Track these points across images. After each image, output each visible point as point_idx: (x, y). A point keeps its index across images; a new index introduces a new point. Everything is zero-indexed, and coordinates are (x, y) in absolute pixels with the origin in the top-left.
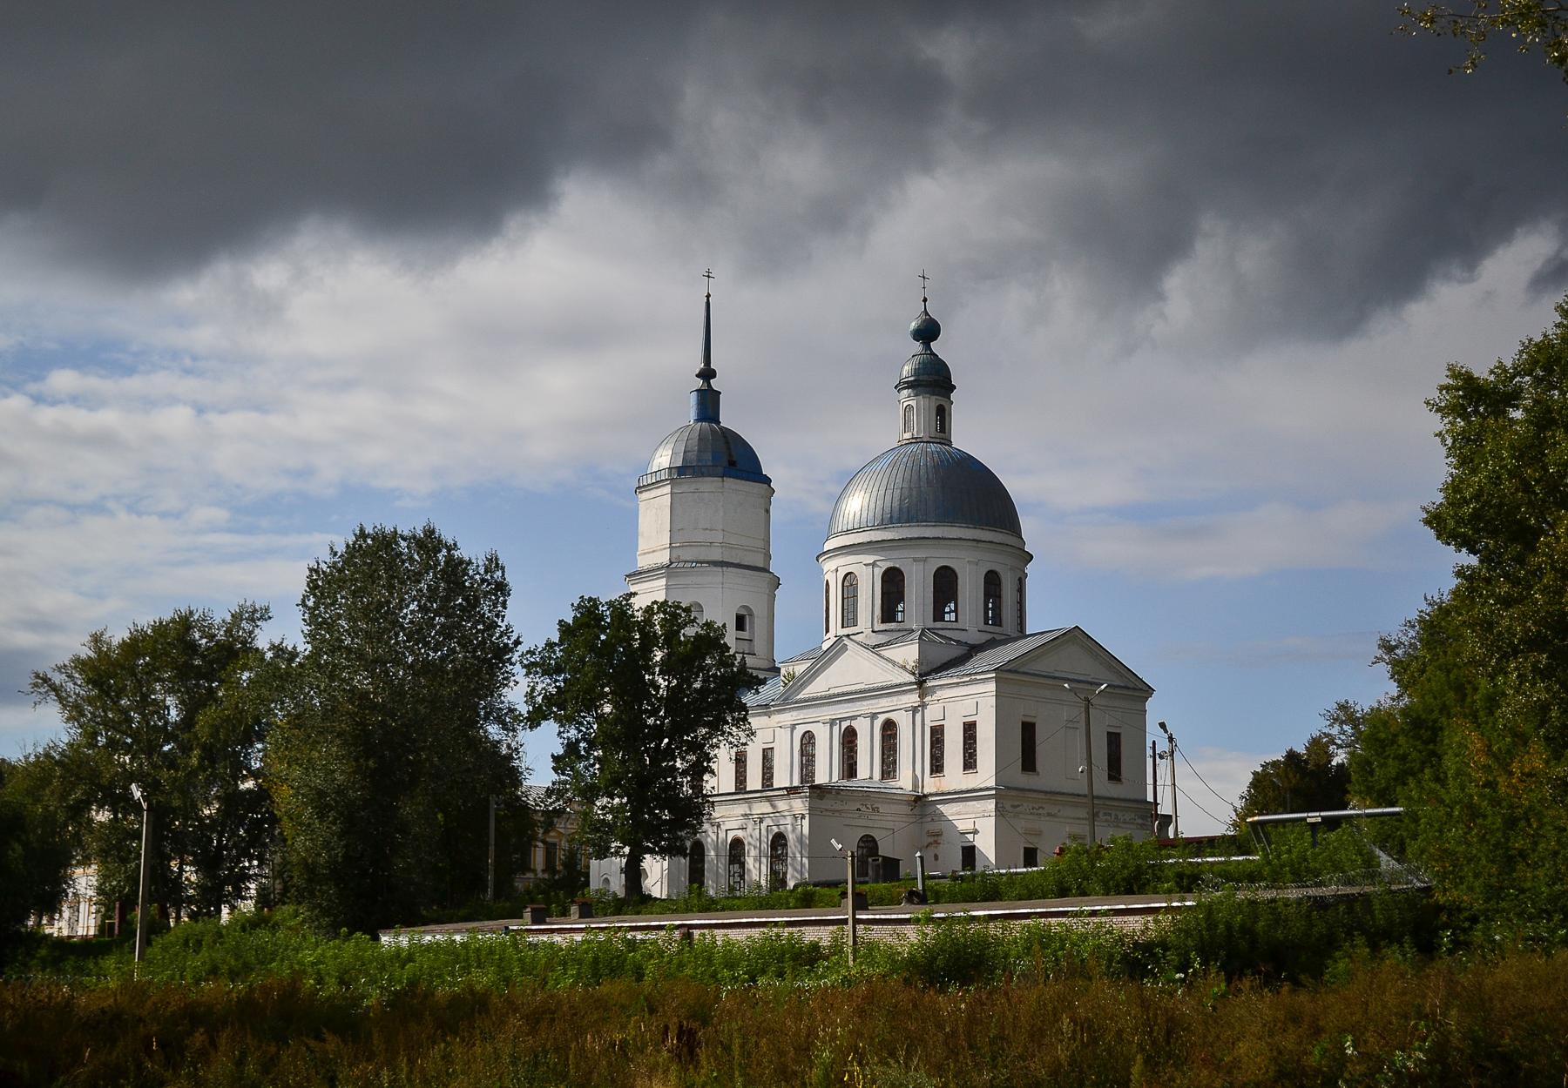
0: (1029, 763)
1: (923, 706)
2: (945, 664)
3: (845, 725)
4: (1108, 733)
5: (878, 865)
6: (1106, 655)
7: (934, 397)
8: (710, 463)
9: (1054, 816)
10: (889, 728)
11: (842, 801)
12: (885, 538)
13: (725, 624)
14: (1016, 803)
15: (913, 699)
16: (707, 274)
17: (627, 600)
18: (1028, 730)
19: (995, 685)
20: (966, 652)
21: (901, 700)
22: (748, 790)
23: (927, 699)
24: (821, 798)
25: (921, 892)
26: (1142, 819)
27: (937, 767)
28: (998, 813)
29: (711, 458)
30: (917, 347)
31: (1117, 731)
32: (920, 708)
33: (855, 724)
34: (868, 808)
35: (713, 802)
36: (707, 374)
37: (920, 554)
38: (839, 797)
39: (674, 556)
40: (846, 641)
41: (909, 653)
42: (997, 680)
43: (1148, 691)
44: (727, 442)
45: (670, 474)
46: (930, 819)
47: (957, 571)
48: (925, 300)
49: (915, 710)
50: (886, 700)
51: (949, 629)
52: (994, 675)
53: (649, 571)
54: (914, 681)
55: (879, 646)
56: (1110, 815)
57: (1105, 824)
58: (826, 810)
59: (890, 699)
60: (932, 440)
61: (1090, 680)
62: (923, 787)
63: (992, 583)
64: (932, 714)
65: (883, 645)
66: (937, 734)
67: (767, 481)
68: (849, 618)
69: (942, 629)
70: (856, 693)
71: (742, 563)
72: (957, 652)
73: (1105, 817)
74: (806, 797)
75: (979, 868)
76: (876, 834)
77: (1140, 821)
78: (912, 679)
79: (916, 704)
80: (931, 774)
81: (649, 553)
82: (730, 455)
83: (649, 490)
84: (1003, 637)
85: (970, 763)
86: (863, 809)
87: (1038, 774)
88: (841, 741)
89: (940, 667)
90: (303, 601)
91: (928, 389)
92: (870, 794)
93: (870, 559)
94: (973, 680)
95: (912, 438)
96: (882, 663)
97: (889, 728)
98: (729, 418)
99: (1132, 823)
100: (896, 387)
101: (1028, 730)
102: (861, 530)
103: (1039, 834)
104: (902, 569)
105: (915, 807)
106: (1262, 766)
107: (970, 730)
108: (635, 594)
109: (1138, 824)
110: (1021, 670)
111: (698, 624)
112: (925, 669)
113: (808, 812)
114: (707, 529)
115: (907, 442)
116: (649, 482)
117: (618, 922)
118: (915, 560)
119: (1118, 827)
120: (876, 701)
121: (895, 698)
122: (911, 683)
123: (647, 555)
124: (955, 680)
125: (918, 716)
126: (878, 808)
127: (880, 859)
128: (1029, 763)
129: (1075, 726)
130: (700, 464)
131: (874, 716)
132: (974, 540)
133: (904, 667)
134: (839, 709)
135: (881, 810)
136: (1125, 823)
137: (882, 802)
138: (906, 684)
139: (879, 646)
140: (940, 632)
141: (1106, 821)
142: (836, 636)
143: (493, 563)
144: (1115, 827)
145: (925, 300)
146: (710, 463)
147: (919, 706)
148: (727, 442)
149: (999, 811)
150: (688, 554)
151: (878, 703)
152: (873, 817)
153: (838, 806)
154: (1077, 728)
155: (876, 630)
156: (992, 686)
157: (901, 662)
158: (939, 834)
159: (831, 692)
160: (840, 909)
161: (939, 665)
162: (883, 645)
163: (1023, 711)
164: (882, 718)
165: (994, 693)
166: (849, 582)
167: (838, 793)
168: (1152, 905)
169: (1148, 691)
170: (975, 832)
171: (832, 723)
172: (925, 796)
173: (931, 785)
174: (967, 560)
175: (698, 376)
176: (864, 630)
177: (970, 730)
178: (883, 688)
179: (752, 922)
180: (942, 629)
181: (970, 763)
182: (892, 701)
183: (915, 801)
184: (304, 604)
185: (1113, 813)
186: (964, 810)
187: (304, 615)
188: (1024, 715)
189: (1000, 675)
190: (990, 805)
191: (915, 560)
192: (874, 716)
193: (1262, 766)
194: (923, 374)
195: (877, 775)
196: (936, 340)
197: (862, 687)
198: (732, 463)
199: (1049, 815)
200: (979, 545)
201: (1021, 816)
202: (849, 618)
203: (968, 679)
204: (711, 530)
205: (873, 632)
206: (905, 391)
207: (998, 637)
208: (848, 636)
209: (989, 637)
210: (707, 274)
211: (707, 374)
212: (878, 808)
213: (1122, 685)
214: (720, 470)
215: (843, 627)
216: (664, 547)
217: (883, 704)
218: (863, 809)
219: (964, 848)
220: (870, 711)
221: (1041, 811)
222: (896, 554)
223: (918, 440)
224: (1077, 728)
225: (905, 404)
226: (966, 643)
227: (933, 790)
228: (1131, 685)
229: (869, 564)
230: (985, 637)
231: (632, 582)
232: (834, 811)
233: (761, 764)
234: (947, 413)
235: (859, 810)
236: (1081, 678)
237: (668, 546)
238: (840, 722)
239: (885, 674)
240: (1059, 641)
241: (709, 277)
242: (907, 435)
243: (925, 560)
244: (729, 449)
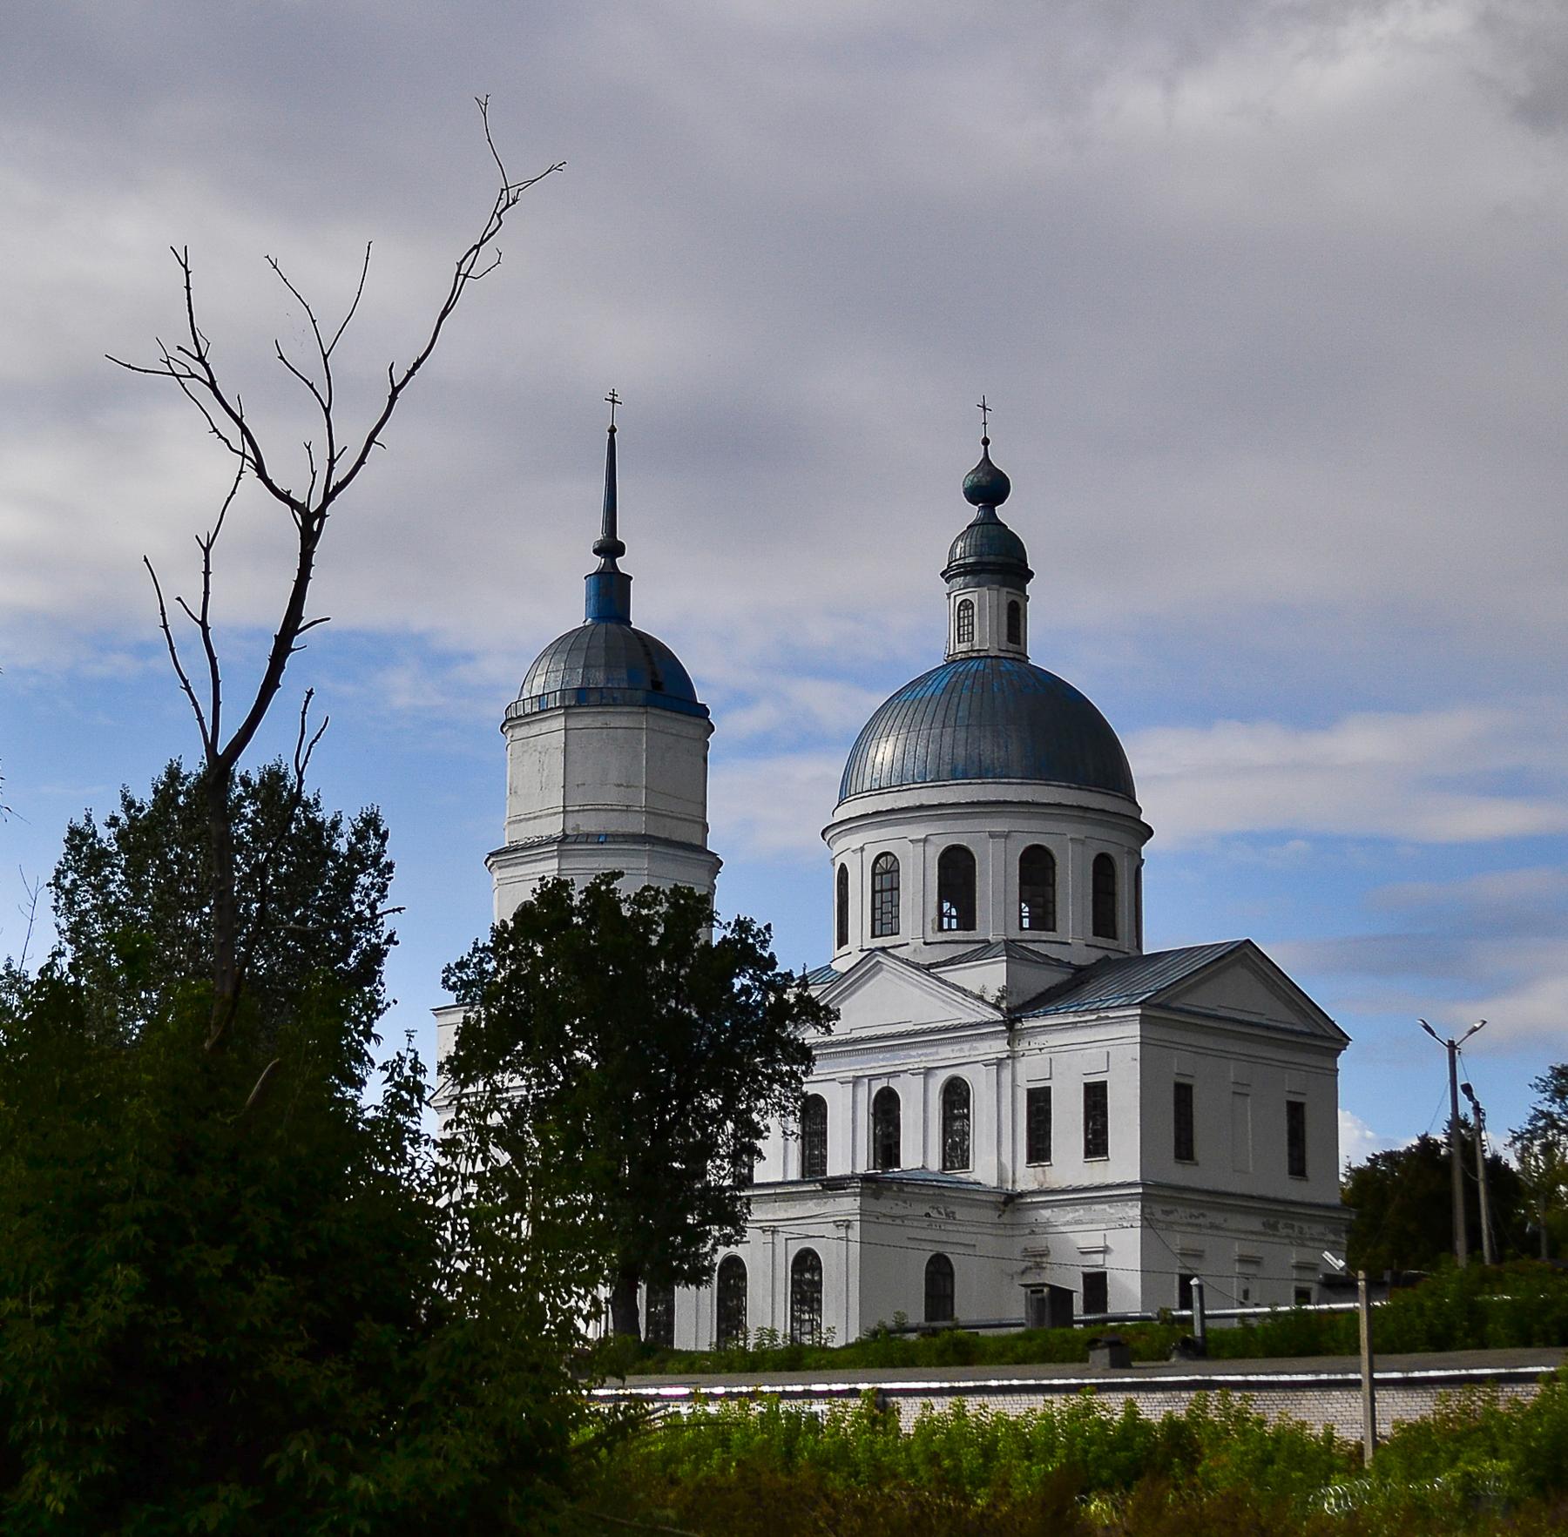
0: (1184, 1150)
1: (1014, 1058)
2: (1042, 994)
3: (877, 1086)
4: (1289, 1103)
5: (1043, 1300)
6: (1286, 985)
7: (1006, 589)
8: (624, 685)
9: (1218, 1228)
10: (956, 1095)
11: (905, 1202)
12: (943, 801)
13: (770, 924)
14: (1168, 1208)
15: (998, 1047)
16: (610, 397)
17: (608, 884)
18: (1183, 1095)
19: (1138, 1026)
20: (1070, 976)
21: (976, 1049)
22: (755, 1181)
23: (1022, 1046)
24: (877, 1195)
25: (1200, 1341)
26: (1335, 1235)
27: (1039, 1150)
28: (1145, 1223)
29: (625, 677)
30: (973, 512)
31: (1299, 1099)
32: (1010, 1061)
33: (894, 1084)
34: (940, 1213)
35: (749, 1198)
36: (610, 548)
37: (1000, 825)
38: (902, 1195)
39: (570, 825)
40: (881, 957)
41: (992, 976)
42: (1144, 1020)
43: (1341, 1040)
44: (648, 654)
45: (563, 698)
46: (1027, 1231)
47: (1054, 852)
48: (986, 442)
49: (999, 1063)
50: (950, 1048)
51: (1045, 942)
52: (1139, 1011)
53: (531, 847)
54: (1002, 1018)
55: (937, 965)
56: (1292, 1227)
57: (1286, 1241)
58: (884, 1215)
59: (957, 1047)
60: (1002, 655)
61: (1265, 1022)
62: (1014, 1182)
63: (1103, 869)
64: (1030, 1071)
65: (945, 964)
66: (1039, 1102)
67: (702, 712)
68: (884, 919)
69: (1034, 941)
70: (900, 1035)
71: (674, 839)
72: (1056, 977)
73: (1286, 1230)
74: (855, 1195)
75: (1114, 1308)
76: (946, 1250)
77: (1332, 1237)
78: (998, 1016)
79: (1004, 1055)
80: (1028, 1162)
81: (529, 819)
82: (654, 673)
83: (528, 723)
84: (1121, 956)
85: (1096, 1145)
86: (934, 1214)
87: (1197, 1164)
88: (871, 1110)
89: (1034, 999)
90: (57, 878)
91: (1000, 577)
92: (942, 1191)
93: (919, 831)
94: (1103, 1018)
95: (973, 651)
96: (946, 991)
97: (956, 1095)
98: (645, 615)
99: (1321, 1240)
100: (943, 574)
101: (1183, 1095)
102: (904, 788)
103: (1198, 1255)
104: (971, 849)
105: (1004, 1211)
106: (1369, 1160)
107: (1096, 1096)
108: (620, 874)
109: (1328, 1241)
110: (1174, 1005)
111: (721, 924)
112: (1017, 1001)
113: (858, 1217)
114: (622, 785)
115: (963, 656)
116: (528, 711)
117: (652, 1386)
118: (992, 835)
119: (1304, 1246)
120: (933, 1050)
121: (966, 1046)
122: (996, 1023)
123: (523, 824)
124: (1071, 1019)
125: (1006, 1075)
126: (953, 1213)
127: (1046, 1290)
128: (1184, 1150)
129: (1244, 1091)
130: (610, 685)
131: (928, 1072)
132: (1079, 807)
133: (981, 998)
134: (870, 1062)
135: (957, 1217)
136: (1313, 1239)
137: (962, 1206)
138: (987, 1024)
139: (937, 965)
140: (1030, 946)
141: (1288, 1236)
142: (862, 950)
143: (371, 822)
144: (1299, 1245)
145: (986, 442)
146: (624, 685)
147: (1008, 1057)
148: (648, 654)
149: (1146, 1219)
150: (589, 824)
151: (937, 1053)
152: (950, 1228)
153: (899, 1209)
154: (1247, 1095)
155: (928, 941)
156: (1134, 1029)
157: (977, 992)
158: (1045, 1253)
159: (855, 1035)
160: (1087, 1365)
161: (1033, 995)
162: (945, 964)
163: (1177, 1065)
164: (941, 1078)
165: (1138, 1040)
166: (886, 873)
167: (901, 1190)
168: (1475, 1372)
169: (1341, 1040)
170: (1105, 1251)
171: (856, 1081)
172: (1021, 1195)
173: (1027, 1178)
174: (1069, 837)
175: (596, 552)
176: (910, 941)
177: (1096, 1096)
178: (947, 1029)
179: (929, 1389)
180: (1034, 941)
181: (1096, 1145)
182: (961, 1050)
183: (1005, 1203)
184: (57, 885)
185: (1296, 1224)
186: (1087, 1218)
187: (56, 901)
188: (1177, 1074)
189: (1148, 1013)
190: (1134, 1211)
191: (992, 835)
192: (928, 1072)
193: (1369, 1160)
194: (989, 555)
195: (935, 1163)
196: (1002, 502)
197: (910, 1027)
198: (657, 685)
199: (1213, 1226)
200: (1088, 815)
201: (1176, 1227)
202: (884, 919)
203: (1094, 1017)
204: (628, 787)
205: (925, 943)
206: (960, 580)
207: (1113, 956)
208: (883, 949)
209: (1100, 954)
210: (610, 397)
211: (610, 548)
212: (953, 1213)
213: (1308, 1030)
214: (640, 695)
215: (873, 936)
216: (555, 810)
217: (947, 1053)
218: (934, 1214)
219: (1086, 1276)
220: (922, 1065)
221: (1201, 1221)
222: (960, 825)
223: (982, 654)
224: (1247, 1095)
225: (959, 600)
226: (1069, 963)
227: (1034, 1186)
228: (1319, 1032)
229: (919, 841)
230: (1094, 955)
231: (500, 864)
232: (894, 1217)
233: (1082, 1128)
234: (1022, 612)
235: (928, 1215)
236: (1255, 1019)
237: (562, 809)
238: (869, 1080)
239: (948, 1008)
240: (1225, 961)
241: (613, 401)
242: (964, 647)
243: (1006, 836)
244: (651, 663)
